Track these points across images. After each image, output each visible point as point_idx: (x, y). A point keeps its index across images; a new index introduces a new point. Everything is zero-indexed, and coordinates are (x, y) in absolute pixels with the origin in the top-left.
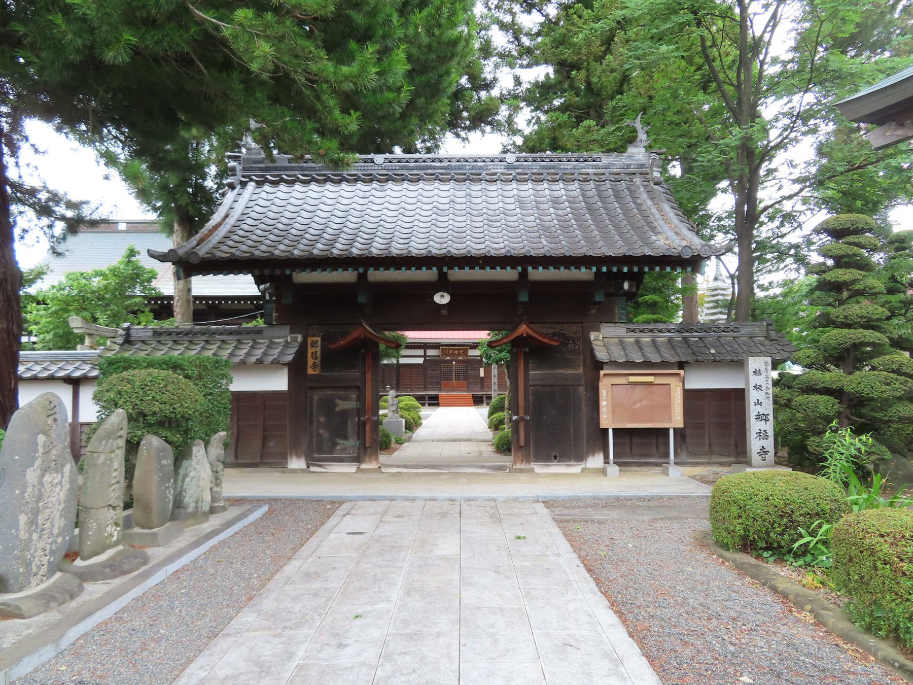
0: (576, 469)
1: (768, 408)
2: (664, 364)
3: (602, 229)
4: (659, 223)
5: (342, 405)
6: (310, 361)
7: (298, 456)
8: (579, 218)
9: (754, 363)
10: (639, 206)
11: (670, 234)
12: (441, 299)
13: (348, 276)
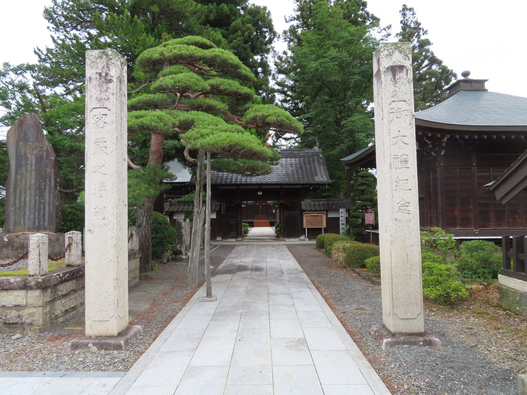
0: (298, 240)
1: (344, 222)
2: (320, 210)
3: (303, 175)
4: (319, 173)
5: (231, 222)
6: (222, 210)
7: (220, 236)
8: (297, 171)
9: (341, 210)
10: (314, 166)
11: (320, 177)
12: (260, 193)
13: (235, 187)
